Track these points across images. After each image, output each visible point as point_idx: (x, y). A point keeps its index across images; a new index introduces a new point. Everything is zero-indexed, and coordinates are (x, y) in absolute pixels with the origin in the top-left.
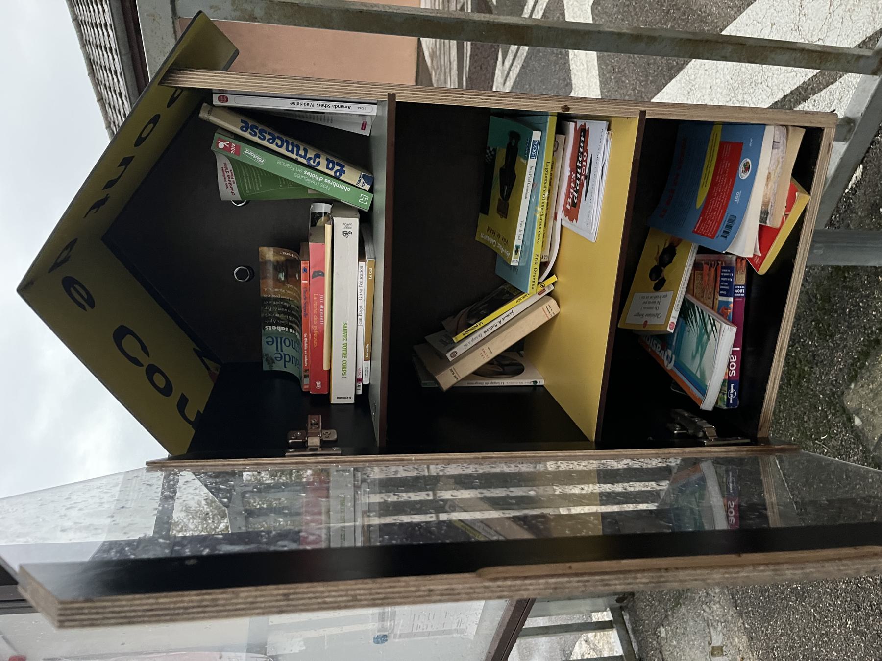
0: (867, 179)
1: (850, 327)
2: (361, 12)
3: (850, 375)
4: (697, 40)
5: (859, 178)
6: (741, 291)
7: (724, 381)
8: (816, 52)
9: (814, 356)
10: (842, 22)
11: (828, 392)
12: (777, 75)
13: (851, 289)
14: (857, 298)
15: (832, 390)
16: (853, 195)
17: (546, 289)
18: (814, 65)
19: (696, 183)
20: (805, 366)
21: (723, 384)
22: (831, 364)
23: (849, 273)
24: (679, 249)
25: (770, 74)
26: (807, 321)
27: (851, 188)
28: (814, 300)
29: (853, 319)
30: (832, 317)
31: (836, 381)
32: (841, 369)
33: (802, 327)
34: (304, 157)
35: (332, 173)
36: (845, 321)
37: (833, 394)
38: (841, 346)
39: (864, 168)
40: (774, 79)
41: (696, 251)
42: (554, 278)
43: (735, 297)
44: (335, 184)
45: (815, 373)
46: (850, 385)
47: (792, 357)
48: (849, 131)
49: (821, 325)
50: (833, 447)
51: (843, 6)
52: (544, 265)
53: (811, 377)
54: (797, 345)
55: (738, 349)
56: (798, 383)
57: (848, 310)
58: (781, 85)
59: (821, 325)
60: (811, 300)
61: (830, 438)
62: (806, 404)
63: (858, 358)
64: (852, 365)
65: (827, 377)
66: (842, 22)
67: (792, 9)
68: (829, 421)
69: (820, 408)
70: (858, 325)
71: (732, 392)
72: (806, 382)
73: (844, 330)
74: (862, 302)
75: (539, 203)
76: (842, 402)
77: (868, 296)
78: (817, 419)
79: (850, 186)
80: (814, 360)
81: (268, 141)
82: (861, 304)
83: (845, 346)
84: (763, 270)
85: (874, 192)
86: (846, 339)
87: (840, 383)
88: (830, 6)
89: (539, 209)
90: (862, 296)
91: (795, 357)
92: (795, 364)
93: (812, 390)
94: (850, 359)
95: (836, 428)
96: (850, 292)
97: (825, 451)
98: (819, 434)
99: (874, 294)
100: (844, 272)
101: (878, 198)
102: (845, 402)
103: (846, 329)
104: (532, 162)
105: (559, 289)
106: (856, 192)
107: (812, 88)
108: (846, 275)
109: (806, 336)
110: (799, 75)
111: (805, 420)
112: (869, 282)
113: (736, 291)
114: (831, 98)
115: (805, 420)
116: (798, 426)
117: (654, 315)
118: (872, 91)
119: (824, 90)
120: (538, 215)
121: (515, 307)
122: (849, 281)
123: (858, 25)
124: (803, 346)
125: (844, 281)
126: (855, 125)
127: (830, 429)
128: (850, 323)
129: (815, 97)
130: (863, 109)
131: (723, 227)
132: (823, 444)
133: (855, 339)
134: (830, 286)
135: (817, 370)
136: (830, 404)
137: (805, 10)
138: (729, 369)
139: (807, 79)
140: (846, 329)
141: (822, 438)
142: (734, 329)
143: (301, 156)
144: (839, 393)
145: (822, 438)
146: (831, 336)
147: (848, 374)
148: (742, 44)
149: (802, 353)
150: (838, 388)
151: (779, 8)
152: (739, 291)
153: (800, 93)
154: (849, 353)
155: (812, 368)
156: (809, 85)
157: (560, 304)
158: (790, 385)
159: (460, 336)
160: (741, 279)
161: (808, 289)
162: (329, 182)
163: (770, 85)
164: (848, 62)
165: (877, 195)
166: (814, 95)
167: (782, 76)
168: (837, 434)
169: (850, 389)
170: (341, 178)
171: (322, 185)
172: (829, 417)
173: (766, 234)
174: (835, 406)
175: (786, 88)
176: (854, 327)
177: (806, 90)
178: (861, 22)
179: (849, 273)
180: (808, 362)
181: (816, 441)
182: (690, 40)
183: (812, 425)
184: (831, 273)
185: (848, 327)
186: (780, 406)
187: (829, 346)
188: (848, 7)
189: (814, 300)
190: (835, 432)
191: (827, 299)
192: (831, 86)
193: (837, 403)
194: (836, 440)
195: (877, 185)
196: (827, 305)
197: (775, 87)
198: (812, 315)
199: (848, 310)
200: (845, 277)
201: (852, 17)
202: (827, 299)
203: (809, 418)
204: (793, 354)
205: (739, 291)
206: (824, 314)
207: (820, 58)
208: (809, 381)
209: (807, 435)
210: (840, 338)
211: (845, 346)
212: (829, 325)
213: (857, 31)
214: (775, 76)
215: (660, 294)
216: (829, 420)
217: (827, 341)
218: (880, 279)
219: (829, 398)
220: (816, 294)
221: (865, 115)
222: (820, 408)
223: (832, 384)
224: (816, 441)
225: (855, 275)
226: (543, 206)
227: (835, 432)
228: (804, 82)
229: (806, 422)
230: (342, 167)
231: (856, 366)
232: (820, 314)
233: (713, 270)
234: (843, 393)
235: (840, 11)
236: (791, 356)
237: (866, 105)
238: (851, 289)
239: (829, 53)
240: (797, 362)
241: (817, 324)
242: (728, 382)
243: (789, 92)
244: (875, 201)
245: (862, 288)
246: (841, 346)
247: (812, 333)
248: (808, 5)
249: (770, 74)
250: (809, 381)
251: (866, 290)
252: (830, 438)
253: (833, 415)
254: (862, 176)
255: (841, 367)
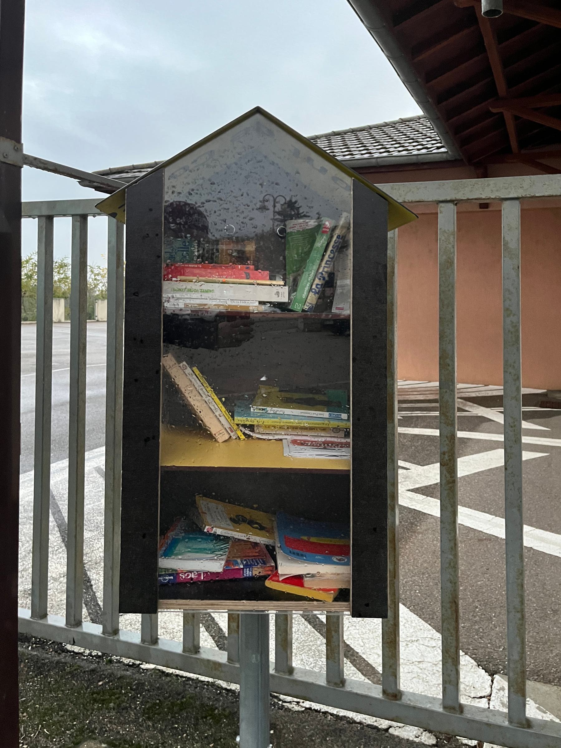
0: (294, 715)
1: (161, 731)
2: (393, 313)
3: (114, 742)
4: (395, 541)
5: (293, 709)
6: (248, 573)
7: (176, 570)
8: (395, 637)
9: (126, 708)
10: (409, 672)
11: (93, 726)
12: (359, 633)
13: (196, 725)
14: (190, 730)
15: (96, 729)
16: (279, 709)
17: (233, 433)
18: (385, 638)
19: (317, 535)
20: (114, 704)
21: (173, 570)
22: (121, 724)
23: (210, 719)
24: (264, 532)
25: (358, 628)
26: (159, 696)
27: (284, 706)
28: (180, 697)
29: (169, 731)
30: (167, 715)
31: (106, 731)
32: (119, 732)
33: (151, 693)
34: (323, 271)
35: (314, 287)
36: (166, 726)
37: (93, 732)
38: (141, 728)
39: (303, 712)
40: (355, 631)
41: (267, 543)
42: (243, 437)
43: (243, 569)
44: (307, 289)
45: (109, 712)
46: (104, 744)
47: (121, 691)
48: (336, 684)
49: (157, 707)
50: (38, 741)
51: (420, 671)
52: (251, 427)
53: (104, 709)
54: (133, 692)
55: (202, 578)
56: (95, 701)
57: (176, 726)
58: (351, 637)
59: (157, 707)
60: (179, 694)
61: (47, 736)
62: (76, 711)
63: (133, 744)
64: (125, 741)
65: (108, 723)
66: (409, 672)
67: (409, 634)
68: (64, 732)
69: (75, 723)
70: (165, 737)
71: (167, 578)
72: (98, 706)
73: (157, 727)
74: (187, 735)
75: (300, 421)
76: (85, 740)
77: (194, 739)
78: (63, 722)
79: (284, 704)
80: (121, 709)
81: (332, 250)
82: (185, 735)
83: (142, 731)
84: (268, 584)
85: (286, 722)
86: (149, 730)
87: (104, 734)
88: (419, 662)
89: (296, 421)
90: (193, 734)
91: (121, 693)
92: (114, 694)
93: (92, 713)
94: (131, 738)
95: (58, 740)
96: (194, 725)
97: (32, 735)
98: (48, 726)
99: (197, 743)
100: (211, 715)
101: (282, 727)
102: (86, 743)
103: (159, 728)
104: (326, 414)
105: (233, 443)
106: (281, 710)
107: (355, 659)
108: (208, 718)
109: (143, 697)
110: (362, 648)
111: (60, 713)
112: (206, 737)
113: (248, 569)
114: (351, 675)
115: (60, 713)
116: (51, 709)
117: (212, 517)
118: (370, 694)
119: (355, 669)
120: (292, 420)
121: (220, 409)
122: (203, 721)
123: (410, 684)
124: (134, 698)
125: (202, 718)
126: (341, 687)
127: (57, 735)
128: (165, 730)
129: (349, 663)
130: (355, 691)
131: (296, 551)
132: (39, 732)
133: (151, 738)
134: (196, 707)
135: (113, 713)
136: (81, 731)
137: (411, 644)
138: (185, 573)
139: (361, 654)
140: (159, 728)
141: (45, 730)
142: (221, 570)
143: (324, 269)
144: (94, 736)
145: (45, 730)
146: (149, 719)
147: (115, 739)
148: (395, 575)
149: (126, 699)
150: (99, 734)
151: (407, 625)
152: (248, 572)
153: (349, 651)
154: (137, 735)
155: (114, 710)
156: (357, 657)
157: (225, 443)
158: (92, 695)
159: (197, 372)
160: (257, 571)
161: (188, 690)
162: (308, 285)
163: (350, 628)
164: (390, 666)
165: (283, 725)
166: (350, 662)
167: (359, 636)
168: (52, 741)
169: (101, 744)
170: (311, 293)
171: (306, 281)
172: (68, 732)
173: (297, 580)
174: (81, 734)
175: (350, 641)
176: (162, 734)
177: (353, 655)
178: (413, 685)
179: (210, 719)
180: (119, 706)
181: (40, 726)
182: (395, 535)
183: (56, 719)
184: (207, 706)
185: (161, 729)
186: (69, 690)
187: (139, 718)
188: (421, 675)
189: (180, 697)
190: (54, 740)
191: (183, 707)
192: (360, 673)
193: (83, 736)
194: (46, 742)
195: (291, 724)
196: (177, 708)
197: (349, 633)
198: (165, 699)
199: (176, 726)
200: (206, 717)
201: (414, 679)
202: (183, 707)
203: (62, 716)
204: (123, 691)
205: (248, 572)
206: (168, 708)
207: (391, 642)
208: (99, 709)
209: (44, 717)
210: (149, 726)
211: (142, 731)
212: (159, 714)
213: (405, 684)
214: (357, 631)
215: (229, 522)
216: (66, 733)
217: (143, 716)
218: (211, 745)
219: (87, 729)
220: (185, 698)
221: (350, 693)
222: (75, 723)
223: (101, 728)
224: (40, 726)
225: (210, 724)
226: (299, 423)
227: (54, 740)
228: (358, 653)
229: (58, 714)
230: (318, 293)
231: (125, 744)
232: (167, 705)
233: (257, 554)
234: (95, 739)
235: (416, 669)
236: (122, 690)
237: (359, 692)
238: (196, 725)
239: (395, 648)
240: (117, 696)
241: (158, 704)
242: (175, 573)
243: (348, 643)
244: (278, 725)
245: (200, 733)
246: (141, 728)
247: (148, 702)
248: (414, 646)
249: (358, 628)
250: (99, 709)
251: (199, 737)
252: (47, 736)
253: (70, 735)
254: (296, 711)
255: (121, 732)
